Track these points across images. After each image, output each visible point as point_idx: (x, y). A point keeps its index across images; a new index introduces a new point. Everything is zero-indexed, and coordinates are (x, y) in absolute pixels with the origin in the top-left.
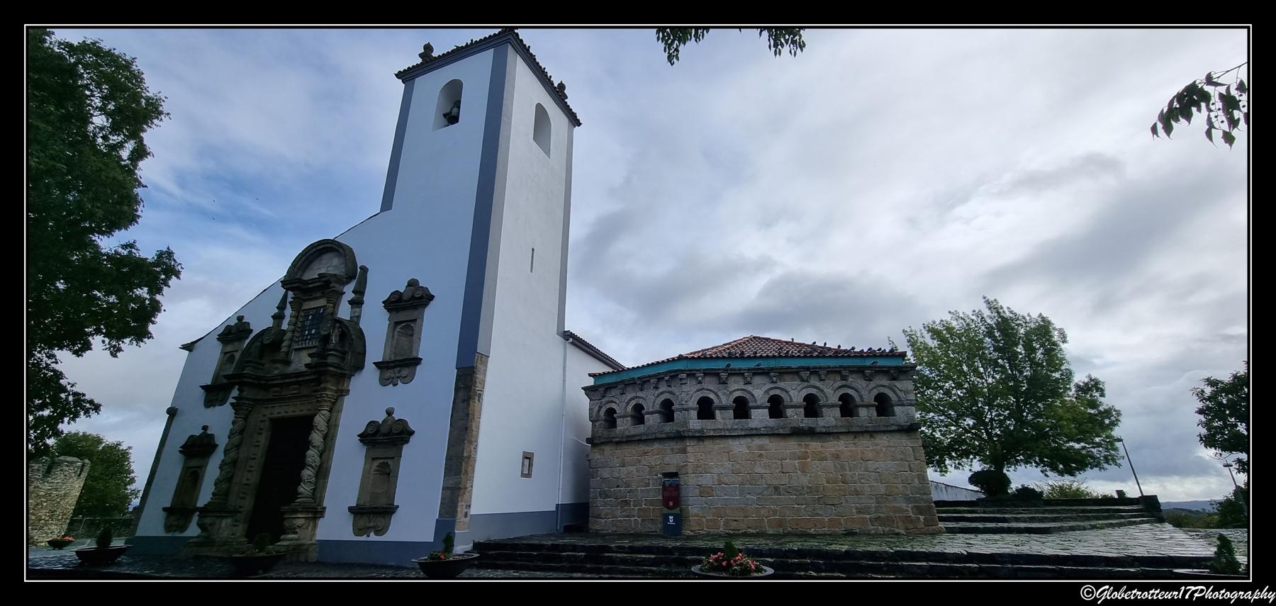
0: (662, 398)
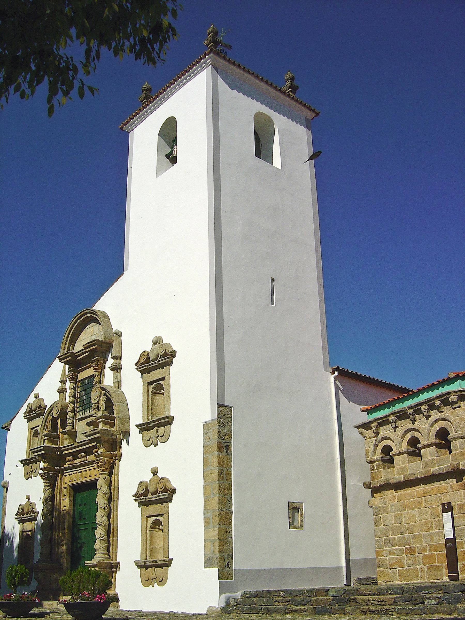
0: (437, 427)
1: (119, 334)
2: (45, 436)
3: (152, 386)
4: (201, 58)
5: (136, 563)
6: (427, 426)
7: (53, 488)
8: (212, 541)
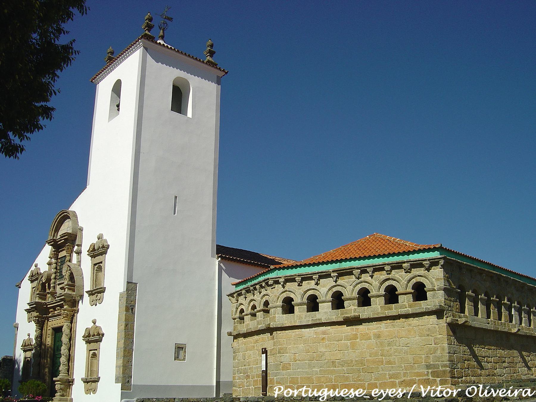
0: (264, 299)
1: (81, 230)
2: (38, 294)
3: (96, 266)
4: (137, 41)
5: (82, 379)
6: (259, 298)
7: (42, 329)
8: (119, 367)
